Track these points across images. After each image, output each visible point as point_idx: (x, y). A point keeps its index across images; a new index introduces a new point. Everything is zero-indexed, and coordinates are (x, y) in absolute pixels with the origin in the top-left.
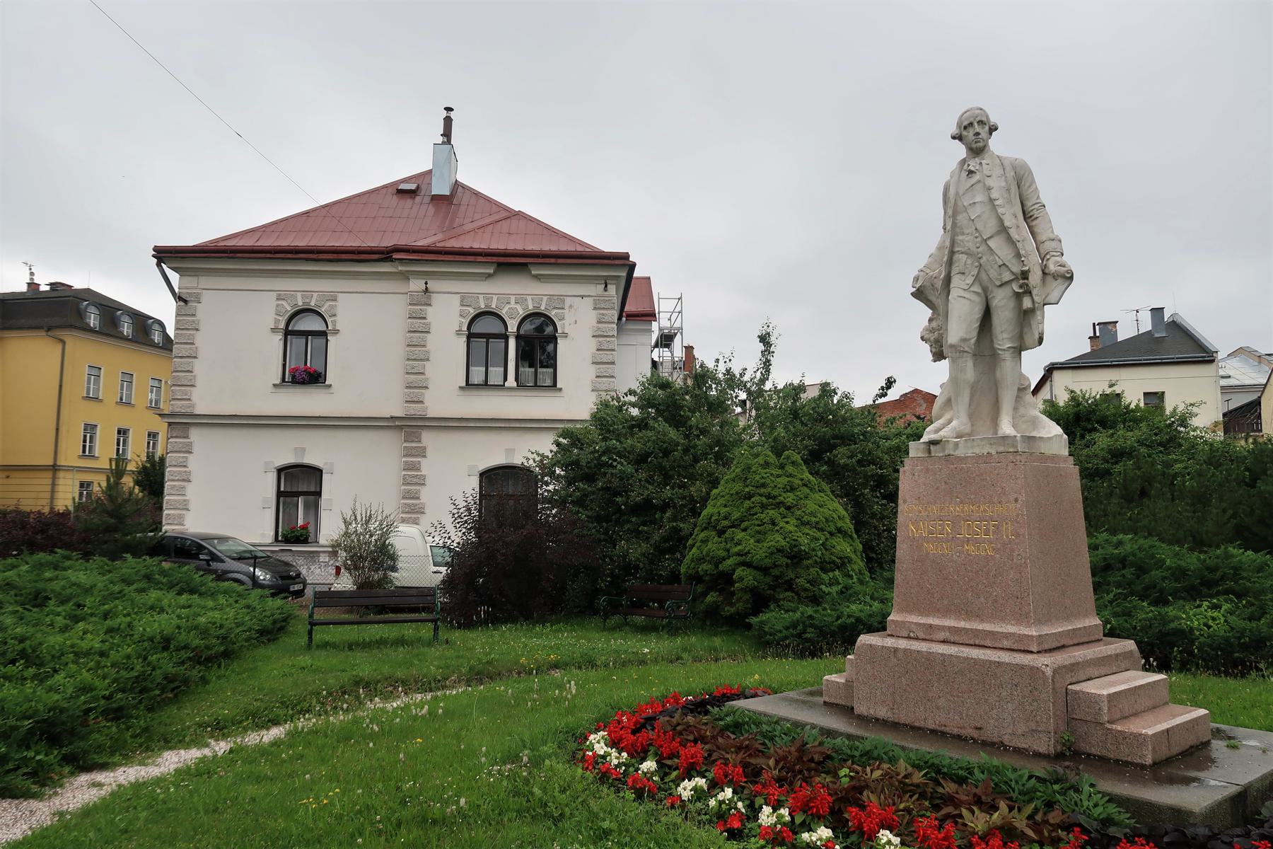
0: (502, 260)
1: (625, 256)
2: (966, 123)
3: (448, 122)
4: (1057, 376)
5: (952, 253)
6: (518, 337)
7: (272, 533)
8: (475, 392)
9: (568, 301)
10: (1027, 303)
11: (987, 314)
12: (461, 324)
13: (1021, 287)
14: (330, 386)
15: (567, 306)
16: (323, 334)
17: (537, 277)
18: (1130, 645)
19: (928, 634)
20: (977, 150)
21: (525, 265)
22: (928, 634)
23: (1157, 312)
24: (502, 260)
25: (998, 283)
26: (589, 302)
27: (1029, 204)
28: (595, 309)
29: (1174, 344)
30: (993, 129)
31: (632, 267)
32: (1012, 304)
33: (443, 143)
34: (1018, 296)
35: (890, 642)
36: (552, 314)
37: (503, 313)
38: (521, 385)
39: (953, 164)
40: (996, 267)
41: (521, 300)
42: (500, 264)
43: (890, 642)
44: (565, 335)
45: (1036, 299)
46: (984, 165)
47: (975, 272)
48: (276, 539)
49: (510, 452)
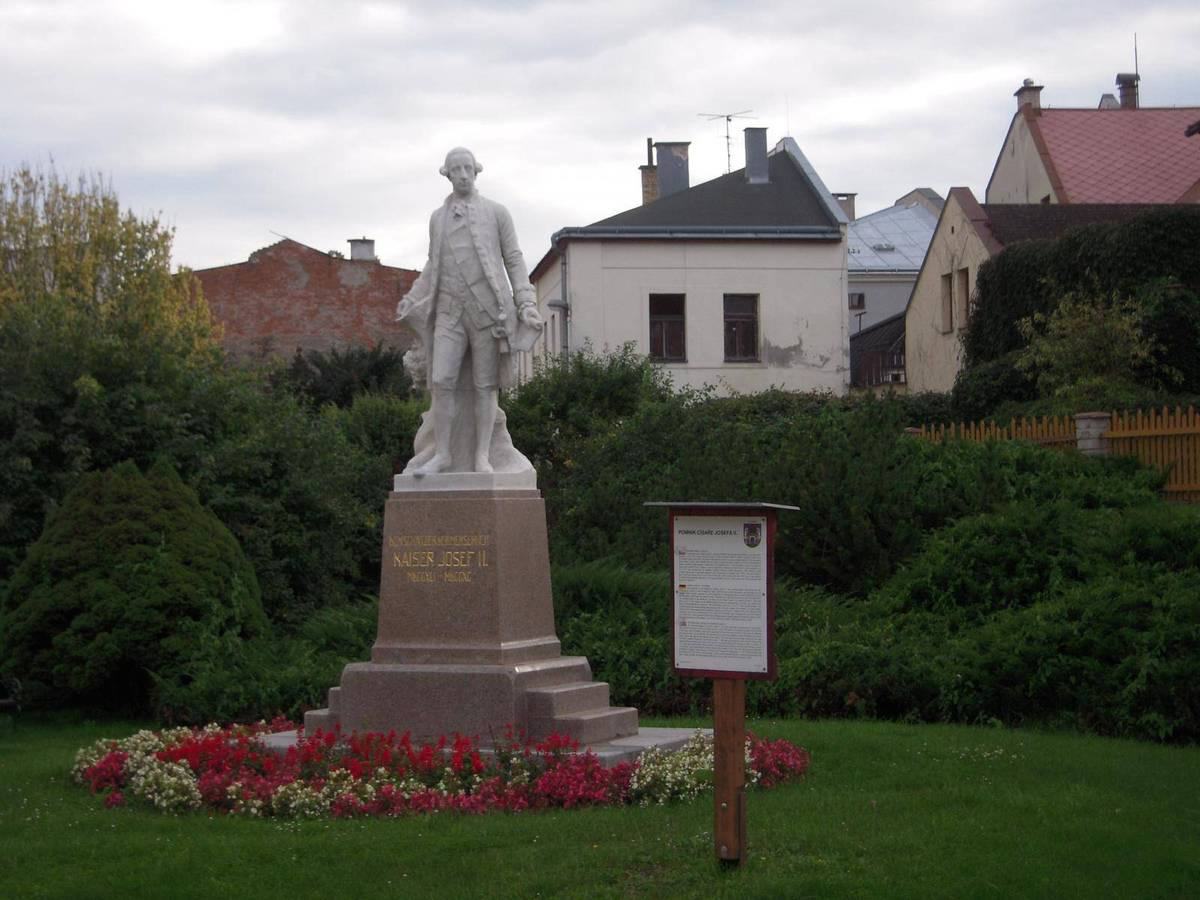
2: (454, 165)
4: (576, 254)
5: (438, 292)
10: (504, 348)
11: (468, 354)
13: (499, 333)
18: (582, 661)
23: (756, 137)
27: (508, 251)
29: (779, 199)
30: (477, 170)
32: (490, 347)
34: (497, 341)
35: (376, 668)
39: (439, 203)
43: (376, 668)
45: (512, 345)
47: (458, 314)
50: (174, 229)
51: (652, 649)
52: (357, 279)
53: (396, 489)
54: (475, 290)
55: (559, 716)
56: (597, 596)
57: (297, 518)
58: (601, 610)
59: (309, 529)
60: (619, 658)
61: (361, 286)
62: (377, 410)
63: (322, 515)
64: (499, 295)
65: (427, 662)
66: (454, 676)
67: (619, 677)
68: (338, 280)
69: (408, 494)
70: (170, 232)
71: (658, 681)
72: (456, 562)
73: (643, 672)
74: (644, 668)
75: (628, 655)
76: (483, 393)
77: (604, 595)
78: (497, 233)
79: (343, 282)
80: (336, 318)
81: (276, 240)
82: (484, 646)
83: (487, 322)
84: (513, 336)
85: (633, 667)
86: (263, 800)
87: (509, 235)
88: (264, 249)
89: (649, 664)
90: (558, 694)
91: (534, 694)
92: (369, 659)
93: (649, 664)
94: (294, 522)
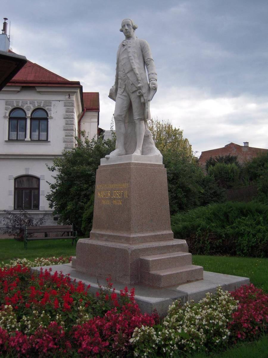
0: (25, 85)
1: (78, 83)
3: (5, 25)
6: (32, 119)
7: (13, 206)
8: (33, 143)
9: (53, 103)
12: (6, 113)
14: (50, 141)
15: (52, 105)
16: (46, 119)
17: (39, 92)
18: (184, 242)
19: (144, 240)
20: (128, 37)
21: (34, 87)
22: (144, 240)
24: (25, 85)
25: (131, 92)
26: (62, 103)
27: (146, 59)
28: (65, 106)
30: (134, 28)
31: (81, 88)
33: (3, 34)
36: (46, 108)
37: (25, 108)
38: (32, 141)
40: (130, 85)
41: (32, 103)
42: (23, 87)
44: (52, 118)
46: (131, 42)
47: (124, 87)
48: (15, 209)
49: (27, 169)
50: (183, 130)
51: (261, 230)
52: (245, 150)
53: (101, 165)
54: (129, 75)
55: (152, 272)
56: (249, 212)
57: (181, 190)
58: (249, 216)
59: (184, 192)
60: (249, 232)
61: (246, 151)
62: (221, 167)
63: (188, 189)
64: (138, 76)
65: (106, 240)
66: (110, 248)
67: (249, 239)
68: (242, 150)
69: (104, 166)
70: (182, 131)
71: (263, 241)
72: (118, 193)
73: (258, 237)
74: (258, 236)
75: (252, 232)
76: (137, 122)
77: (251, 211)
78: (141, 52)
79: (243, 150)
80: (241, 157)
81: (230, 143)
82: (125, 235)
83: (134, 89)
84: (146, 94)
85: (254, 236)
86: (6, 309)
87: (146, 52)
88: (227, 145)
89: (260, 235)
90: (153, 261)
91: (142, 260)
92: (89, 237)
93: (260, 235)
94: (180, 191)
